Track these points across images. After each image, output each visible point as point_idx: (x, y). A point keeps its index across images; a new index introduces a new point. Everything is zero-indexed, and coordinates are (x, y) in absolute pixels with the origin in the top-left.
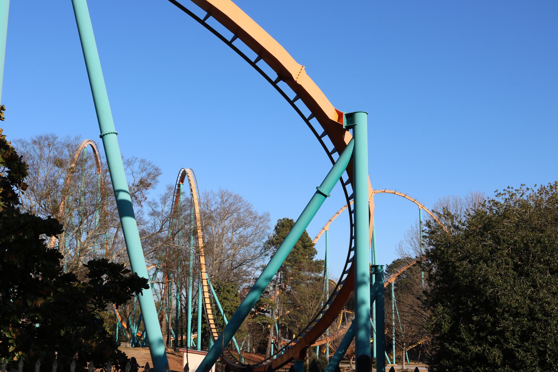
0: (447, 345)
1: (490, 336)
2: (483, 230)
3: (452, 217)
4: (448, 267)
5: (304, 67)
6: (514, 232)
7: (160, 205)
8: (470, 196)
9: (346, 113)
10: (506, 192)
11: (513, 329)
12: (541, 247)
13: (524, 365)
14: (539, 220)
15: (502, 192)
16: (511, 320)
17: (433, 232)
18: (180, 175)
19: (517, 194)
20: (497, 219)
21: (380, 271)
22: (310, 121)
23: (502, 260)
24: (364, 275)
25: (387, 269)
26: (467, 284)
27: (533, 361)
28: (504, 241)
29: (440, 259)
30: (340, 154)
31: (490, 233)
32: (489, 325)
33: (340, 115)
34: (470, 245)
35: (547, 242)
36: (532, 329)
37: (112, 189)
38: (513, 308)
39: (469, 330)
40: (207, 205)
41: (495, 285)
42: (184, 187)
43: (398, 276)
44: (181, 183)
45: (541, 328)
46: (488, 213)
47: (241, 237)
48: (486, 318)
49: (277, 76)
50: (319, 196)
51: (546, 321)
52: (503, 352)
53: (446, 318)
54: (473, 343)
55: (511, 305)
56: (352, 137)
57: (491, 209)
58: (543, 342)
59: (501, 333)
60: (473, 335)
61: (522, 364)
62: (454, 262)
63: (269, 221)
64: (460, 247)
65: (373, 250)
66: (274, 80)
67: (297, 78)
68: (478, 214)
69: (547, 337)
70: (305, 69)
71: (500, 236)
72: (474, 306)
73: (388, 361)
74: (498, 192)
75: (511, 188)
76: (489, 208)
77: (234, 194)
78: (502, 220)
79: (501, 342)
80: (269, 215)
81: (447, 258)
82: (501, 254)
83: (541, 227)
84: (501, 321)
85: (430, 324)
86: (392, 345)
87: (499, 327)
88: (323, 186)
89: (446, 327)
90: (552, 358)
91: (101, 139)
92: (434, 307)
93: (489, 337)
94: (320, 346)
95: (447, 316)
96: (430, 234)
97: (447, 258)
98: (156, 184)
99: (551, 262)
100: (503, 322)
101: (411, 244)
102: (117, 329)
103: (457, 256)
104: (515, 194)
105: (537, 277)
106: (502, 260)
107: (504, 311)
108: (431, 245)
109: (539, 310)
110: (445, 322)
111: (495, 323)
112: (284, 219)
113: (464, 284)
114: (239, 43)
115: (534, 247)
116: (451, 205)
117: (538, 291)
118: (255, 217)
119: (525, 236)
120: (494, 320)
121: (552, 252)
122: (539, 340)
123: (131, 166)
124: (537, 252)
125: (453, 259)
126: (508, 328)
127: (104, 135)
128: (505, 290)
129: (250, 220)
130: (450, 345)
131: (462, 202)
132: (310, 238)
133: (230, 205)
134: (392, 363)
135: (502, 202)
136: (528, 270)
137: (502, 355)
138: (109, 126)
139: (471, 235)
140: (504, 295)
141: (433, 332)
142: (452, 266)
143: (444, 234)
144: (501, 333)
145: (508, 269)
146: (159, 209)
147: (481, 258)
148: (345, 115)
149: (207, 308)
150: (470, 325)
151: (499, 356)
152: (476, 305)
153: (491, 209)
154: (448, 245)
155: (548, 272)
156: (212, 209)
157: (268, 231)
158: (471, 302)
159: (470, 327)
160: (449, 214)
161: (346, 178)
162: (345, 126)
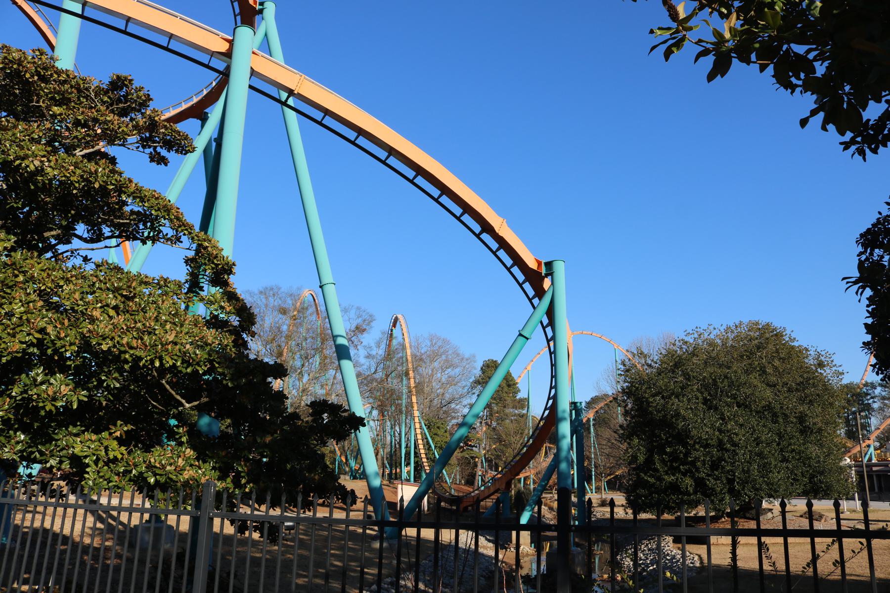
17: (628, 371)
24: (564, 411)
30: (540, 299)
32: (682, 456)
33: (539, 263)
36: (721, 459)
39: (663, 461)
45: (729, 458)
51: (734, 451)
54: (667, 473)
58: (732, 471)
59: (693, 463)
60: (666, 465)
61: (713, 491)
63: (475, 362)
66: (477, 232)
72: (667, 439)
74: (687, 332)
87: (691, 458)
89: (641, 458)
93: (681, 467)
107: (695, 442)
109: (727, 441)
111: (687, 454)
112: (488, 360)
113: (658, 418)
115: (722, 383)
123: (348, 313)
138: (327, 277)
143: (638, 373)
144: (693, 463)
146: (374, 353)
147: (673, 394)
152: (669, 437)
153: (681, 348)
155: (735, 405)
157: (475, 371)
158: (664, 435)
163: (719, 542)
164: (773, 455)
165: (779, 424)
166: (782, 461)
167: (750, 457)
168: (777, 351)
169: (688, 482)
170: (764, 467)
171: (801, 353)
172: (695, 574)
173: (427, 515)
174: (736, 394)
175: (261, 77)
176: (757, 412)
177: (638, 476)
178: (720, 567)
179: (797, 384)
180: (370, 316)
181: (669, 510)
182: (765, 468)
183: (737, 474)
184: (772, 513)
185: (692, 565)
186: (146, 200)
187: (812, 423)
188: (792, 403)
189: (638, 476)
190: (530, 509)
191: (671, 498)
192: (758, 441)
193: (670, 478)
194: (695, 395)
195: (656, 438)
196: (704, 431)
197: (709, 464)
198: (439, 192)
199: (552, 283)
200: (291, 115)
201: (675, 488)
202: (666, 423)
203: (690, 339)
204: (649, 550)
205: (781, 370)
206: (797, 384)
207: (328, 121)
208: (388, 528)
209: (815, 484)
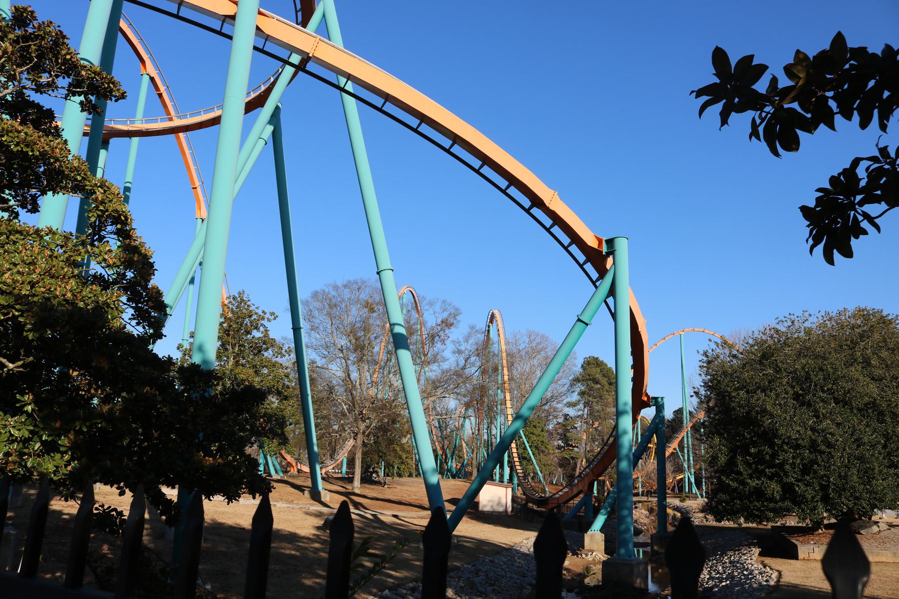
0: (724, 478)
4: (724, 397)
5: (557, 192)
9: (605, 239)
11: (793, 461)
15: (784, 319)
18: (489, 317)
24: (626, 404)
32: (768, 457)
33: (600, 241)
39: (748, 465)
45: (823, 461)
50: (579, 323)
51: (830, 453)
54: (751, 477)
57: (772, 337)
58: (825, 475)
59: (781, 466)
60: (751, 468)
61: (803, 498)
63: (575, 359)
72: (751, 438)
87: (779, 460)
89: (723, 459)
93: (767, 470)
95: (723, 448)
107: (783, 442)
109: (822, 442)
111: (774, 456)
112: (589, 357)
113: (741, 415)
115: (816, 376)
120: (772, 453)
133: (537, 344)
138: (385, 262)
144: (781, 466)
146: (463, 348)
150: (748, 457)
152: (754, 436)
153: (772, 337)
157: (575, 369)
158: (748, 433)
160: (725, 342)
163: (811, 557)
164: (877, 458)
165: (886, 423)
166: (889, 467)
167: (849, 461)
168: (885, 341)
169: (774, 488)
170: (865, 472)
172: (763, 595)
173: (511, 516)
174: (832, 388)
175: (274, 41)
176: (859, 410)
177: (719, 479)
178: (798, 587)
180: (456, 309)
181: (754, 519)
182: (867, 476)
183: (832, 480)
184: (879, 526)
185: (765, 583)
186: (827, 355)
189: (719, 479)
190: (605, 512)
191: (755, 506)
192: (859, 442)
193: (753, 483)
194: (785, 389)
195: (740, 437)
196: (793, 430)
197: (799, 468)
198: (480, 163)
199: (614, 263)
200: (350, 102)
201: (759, 493)
202: (750, 420)
203: (782, 328)
204: (731, 562)
205: (889, 362)
207: (389, 108)
208: (249, 545)
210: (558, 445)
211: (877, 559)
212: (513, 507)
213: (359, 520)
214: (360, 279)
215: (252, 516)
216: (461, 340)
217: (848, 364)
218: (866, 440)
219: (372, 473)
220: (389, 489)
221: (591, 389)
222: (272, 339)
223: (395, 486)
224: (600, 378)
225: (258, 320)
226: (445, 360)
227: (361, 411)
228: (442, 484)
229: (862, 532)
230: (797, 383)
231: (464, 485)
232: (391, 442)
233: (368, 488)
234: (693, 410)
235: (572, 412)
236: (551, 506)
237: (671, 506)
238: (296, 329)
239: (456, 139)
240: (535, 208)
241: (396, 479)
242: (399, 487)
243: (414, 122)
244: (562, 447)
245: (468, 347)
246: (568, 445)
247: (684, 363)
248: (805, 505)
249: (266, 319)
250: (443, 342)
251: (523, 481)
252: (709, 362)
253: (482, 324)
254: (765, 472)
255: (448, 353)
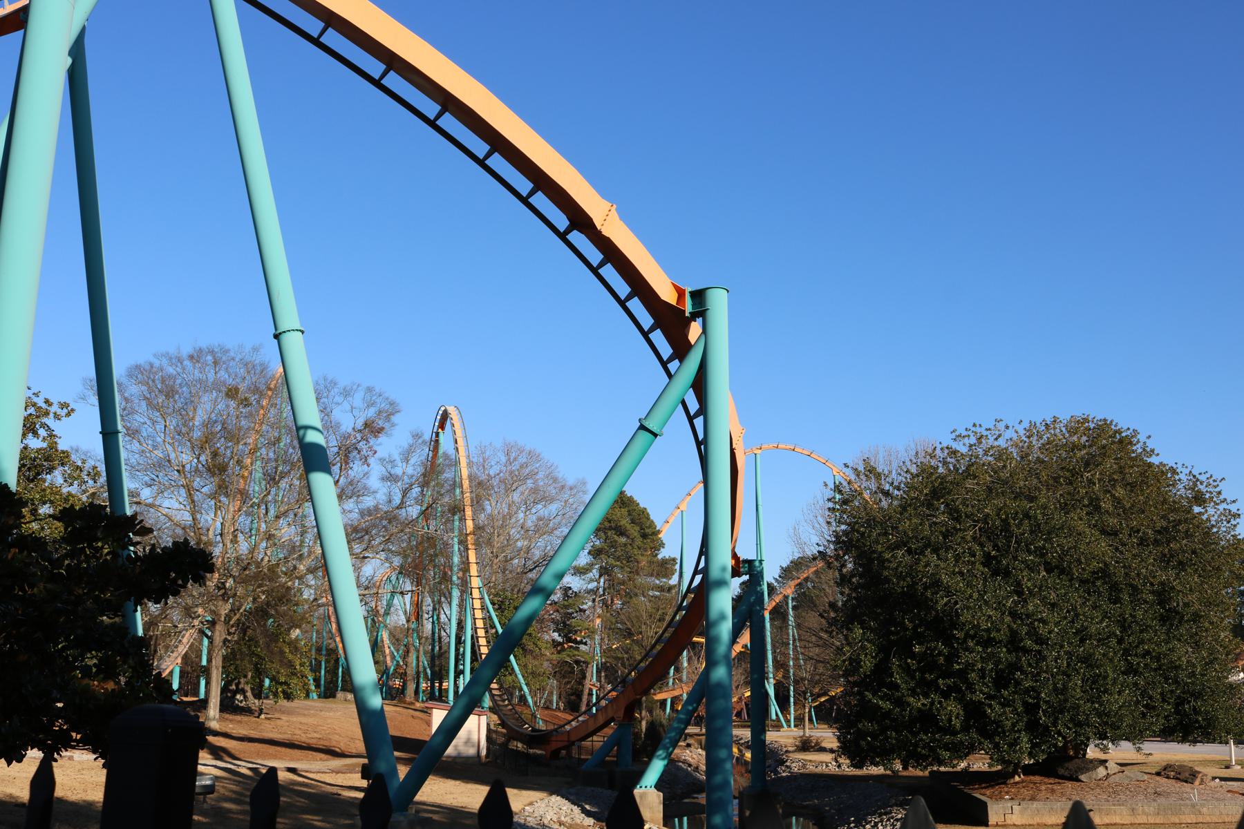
0: (869, 695)
1: (942, 679)
2: (932, 498)
3: (878, 476)
4: (871, 560)
5: (615, 206)
6: (985, 501)
7: (400, 464)
8: (913, 446)
9: (690, 289)
10: (970, 433)
11: (982, 666)
12: (1031, 525)
13: (1000, 730)
14: (1027, 481)
15: (964, 433)
16: (979, 652)
17: (845, 502)
18: (439, 417)
19: (989, 436)
20: (955, 478)
21: (759, 569)
22: (628, 304)
23: (963, 548)
25: (782, 573)
26: (904, 591)
27: (1017, 722)
28: (967, 516)
29: (857, 548)
31: (942, 503)
33: (681, 293)
34: (908, 523)
35: (1040, 517)
36: (1015, 667)
37: (291, 424)
38: (983, 630)
39: (907, 670)
40: (484, 467)
41: (951, 592)
42: (445, 440)
43: (800, 584)
44: (440, 430)
45: (1030, 665)
46: (941, 470)
47: (540, 519)
48: (935, 648)
49: (568, 223)
50: (643, 434)
51: (1039, 652)
52: (965, 709)
53: (868, 649)
54: (914, 693)
55: (978, 626)
56: (701, 331)
57: (945, 463)
58: (1033, 689)
59: (962, 674)
60: (913, 678)
61: (998, 726)
62: (881, 553)
64: (892, 527)
65: (759, 543)
66: (562, 229)
67: (602, 225)
68: (923, 471)
69: (1041, 680)
70: (617, 210)
71: (961, 507)
72: (915, 628)
73: (782, 723)
74: (957, 433)
75: (978, 426)
76: (941, 460)
77: (528, 448)
78: (964, 480)
79: (962, 690)
80: (585, 484)
81: (870, 545)
82: (962, 538)
83: (1030, 493)
84: (961, 653)
85: (839, 659)
86: (789, 696)
87: (959, 664)
88: (652, 414)
89: (868, 664)
90: (1049, 716)
91: (276, 341)
92: (848, 629)
93: (941, 681)
94: (672, 699)
95: (869, 645)
96: (841, 506)
97: (870, 545)
98: (392, 428)
99: (1047, 550)
100: (964, 654)
101: (813, 526)
102: (340, 670)
103: (888, 541)
104: (987, 436)
105: (1023, 577)
106: (963, 548)
107: (967, 635)
108: (843, 524)
109: (1026, 634)
110: (866, 657)
111: (952, 657)
114: (498, 162)
115: (1019, 526)
116: (881, 460)
117: (1025, 601)
118: (563, 487)
119: (1002, 507)
121: (1049, 533)
122: (1026, 686)
123: (350, 399)
124: (1024, 534)
125: (879, 548)
126: (974, 665)
127: (280, 334)
128: (968, 599)
129: (554, 491)
130: (873, 696)
131: (899, 456)
132: (652, 522)
133: (522, 466)
134: (789, 726)
135: (964, 450)
136: (1008, 564)
137: (962, 713)
138: (289, 317)
139: (910, 505)
140: (968, 608)
141: (846, 674)
142: (878, 559)
144: (962, 674)
145: (973, 563)
146: (398, 471)
147: (926, 546)
148: (690, 292)
149: (479, 635)
150: (909, 661)
151: (958, 714)
152: (920, 626)
153: (945, 463)
154: (871, 522)
155: (1042, 568)
156: (492, 473)
159: (908, 664)
161: (693, 406)
162: (690, 313)
163: (1009, 822)
164: (1111, 660)
167: (1068, 665)
168: (1121, 470)
170: (1093, 683)
171: (1164, 475)
173: (485, 764)
174: (1044, 547)
176: (1083, 582)
179: (1155, 531)
181: (917, 762)
182: (1096, 686)
184: (1106, 768)
187: (1181, 604)
188: (1148, 568)
190: (664, 755)
193: (918, 703)
194: (969, 549)
199: (705, 331)
201: (927, 719)
202: (914, 600)
206: (1155, 531)
209: (1186, 715)
210: (553, 641)
211: (1107, 820)
212: (488, 749)
213: (229, 779)
214: (219, 345)
215: (30, 779)
216: (396, 457)
217: (1065, 508)
218: (1093, 629)
219: (235, 693)
220: (268, 722)
221: (613, 545)
222: (63, 452)
223: (277, 715)
224: (629, 526)
225: (38, 417)
226: (366, 491)
227: (223, 584)
228: (386, 708)
229: (1082, 777)
230: (989, 538)
231: (396, 712)
232: (274, 637)
233: (231, 721)
234: (773, 581)
235: (575, 583)
236: (554, 746)
237: (742, 741)
238: (109, 435)
239: (449, 103)
240: (575, 232)
241: (283, 703)
242: (284, 718)
243: (430, 108)
244: (560, 644)
245: (412, 469)
246: (570, 640)
247: (760, 503)
248: (1001, 738)
249: (52, 415)
250: (365, 460)
251: (501, 703)
252: (844, 500)
253: (428, 430)
254: (938, 685)
255: (374, 482)
